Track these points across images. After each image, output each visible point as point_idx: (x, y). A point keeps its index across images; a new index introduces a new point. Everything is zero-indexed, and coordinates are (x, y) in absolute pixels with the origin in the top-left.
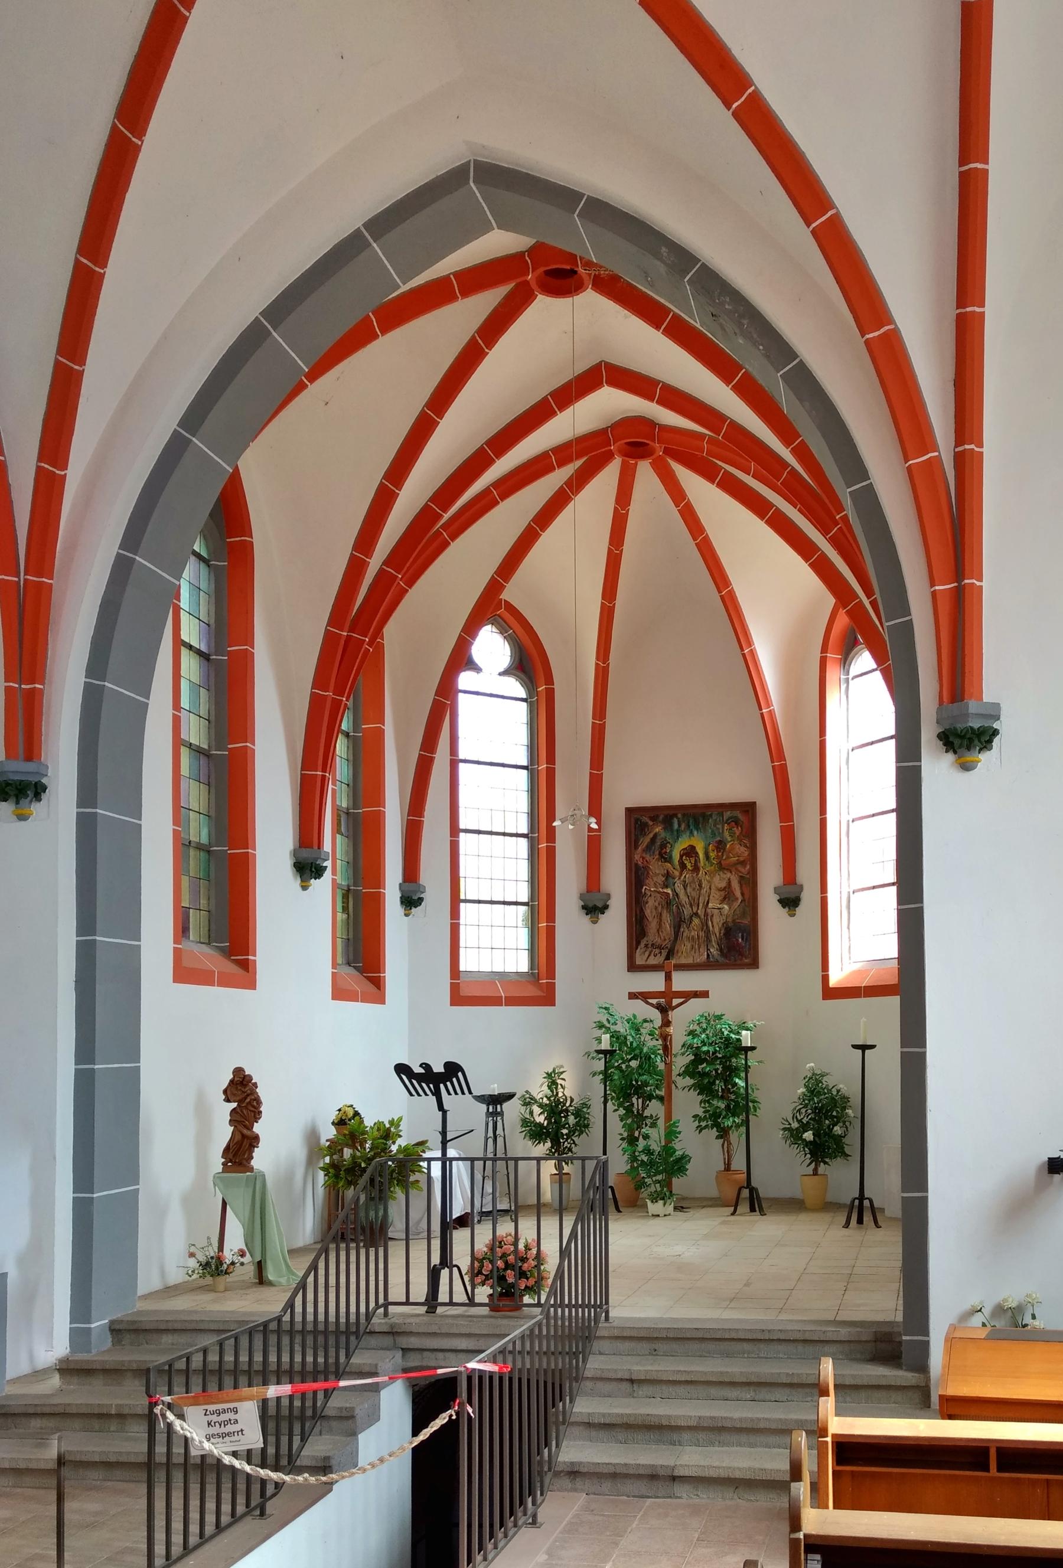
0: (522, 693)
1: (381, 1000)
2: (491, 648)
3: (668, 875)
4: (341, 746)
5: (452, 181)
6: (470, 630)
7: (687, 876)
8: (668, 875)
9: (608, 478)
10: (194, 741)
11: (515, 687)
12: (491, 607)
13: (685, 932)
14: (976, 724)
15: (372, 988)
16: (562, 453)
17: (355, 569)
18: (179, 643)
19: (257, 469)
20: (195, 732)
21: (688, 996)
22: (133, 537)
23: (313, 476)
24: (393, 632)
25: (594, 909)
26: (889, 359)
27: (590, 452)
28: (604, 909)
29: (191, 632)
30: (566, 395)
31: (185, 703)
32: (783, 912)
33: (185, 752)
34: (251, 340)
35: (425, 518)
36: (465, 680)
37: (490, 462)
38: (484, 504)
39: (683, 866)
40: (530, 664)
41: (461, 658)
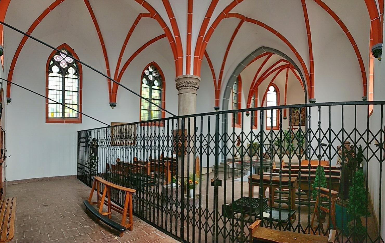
0: (276, 93)
1: (257, 129)
2: (272, 88)
3: (294, 115)
4: (252, 101)
5: (261, 47)
6: (269, 87)
7: (297, 115)
8: (294, 115)
9: (285, 71)
10: (235, 102)
11: (275, 93)
12: (271, 84)
13: (297, 121)
14: (313, 101)
15: (255, 128)
16: (278, 68)
17: (253, 83)
18: (233, 93)
19: (242, 74)
20: (235, 101)
21: (295, 129)
22: (224, 97)
23: (248, 75)
24: (259, 87)
25: (285, 119)
26: (303, 65)
27: (282, 68)
28: (286, 118)
29: (234, 91)
30: (278, 62)
31: (233, 98)
32: (284, 120)
33: (233, 104)
34: (240, 64)
35: (264, 74)
36: (268, 92)
37: (269, 70)
38: (272, 72)
39: (296, 114)
40: (277, 90)
41: (268, 90)
